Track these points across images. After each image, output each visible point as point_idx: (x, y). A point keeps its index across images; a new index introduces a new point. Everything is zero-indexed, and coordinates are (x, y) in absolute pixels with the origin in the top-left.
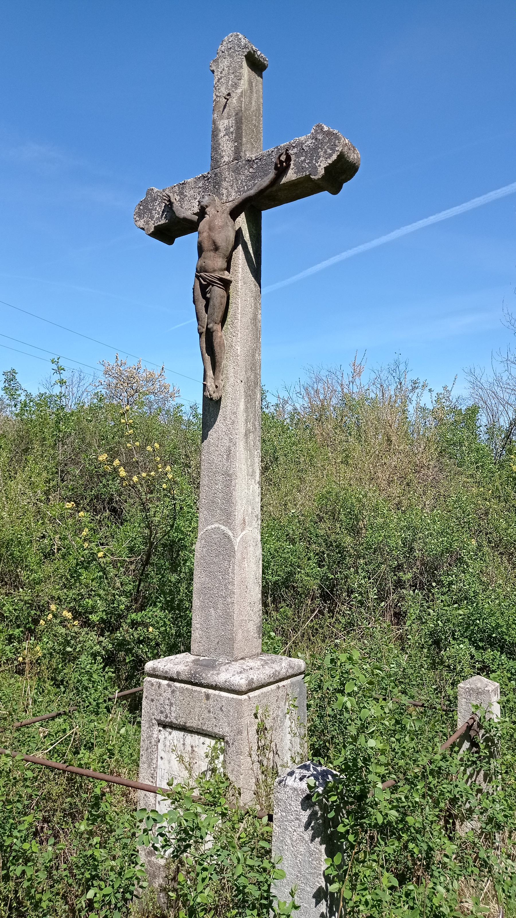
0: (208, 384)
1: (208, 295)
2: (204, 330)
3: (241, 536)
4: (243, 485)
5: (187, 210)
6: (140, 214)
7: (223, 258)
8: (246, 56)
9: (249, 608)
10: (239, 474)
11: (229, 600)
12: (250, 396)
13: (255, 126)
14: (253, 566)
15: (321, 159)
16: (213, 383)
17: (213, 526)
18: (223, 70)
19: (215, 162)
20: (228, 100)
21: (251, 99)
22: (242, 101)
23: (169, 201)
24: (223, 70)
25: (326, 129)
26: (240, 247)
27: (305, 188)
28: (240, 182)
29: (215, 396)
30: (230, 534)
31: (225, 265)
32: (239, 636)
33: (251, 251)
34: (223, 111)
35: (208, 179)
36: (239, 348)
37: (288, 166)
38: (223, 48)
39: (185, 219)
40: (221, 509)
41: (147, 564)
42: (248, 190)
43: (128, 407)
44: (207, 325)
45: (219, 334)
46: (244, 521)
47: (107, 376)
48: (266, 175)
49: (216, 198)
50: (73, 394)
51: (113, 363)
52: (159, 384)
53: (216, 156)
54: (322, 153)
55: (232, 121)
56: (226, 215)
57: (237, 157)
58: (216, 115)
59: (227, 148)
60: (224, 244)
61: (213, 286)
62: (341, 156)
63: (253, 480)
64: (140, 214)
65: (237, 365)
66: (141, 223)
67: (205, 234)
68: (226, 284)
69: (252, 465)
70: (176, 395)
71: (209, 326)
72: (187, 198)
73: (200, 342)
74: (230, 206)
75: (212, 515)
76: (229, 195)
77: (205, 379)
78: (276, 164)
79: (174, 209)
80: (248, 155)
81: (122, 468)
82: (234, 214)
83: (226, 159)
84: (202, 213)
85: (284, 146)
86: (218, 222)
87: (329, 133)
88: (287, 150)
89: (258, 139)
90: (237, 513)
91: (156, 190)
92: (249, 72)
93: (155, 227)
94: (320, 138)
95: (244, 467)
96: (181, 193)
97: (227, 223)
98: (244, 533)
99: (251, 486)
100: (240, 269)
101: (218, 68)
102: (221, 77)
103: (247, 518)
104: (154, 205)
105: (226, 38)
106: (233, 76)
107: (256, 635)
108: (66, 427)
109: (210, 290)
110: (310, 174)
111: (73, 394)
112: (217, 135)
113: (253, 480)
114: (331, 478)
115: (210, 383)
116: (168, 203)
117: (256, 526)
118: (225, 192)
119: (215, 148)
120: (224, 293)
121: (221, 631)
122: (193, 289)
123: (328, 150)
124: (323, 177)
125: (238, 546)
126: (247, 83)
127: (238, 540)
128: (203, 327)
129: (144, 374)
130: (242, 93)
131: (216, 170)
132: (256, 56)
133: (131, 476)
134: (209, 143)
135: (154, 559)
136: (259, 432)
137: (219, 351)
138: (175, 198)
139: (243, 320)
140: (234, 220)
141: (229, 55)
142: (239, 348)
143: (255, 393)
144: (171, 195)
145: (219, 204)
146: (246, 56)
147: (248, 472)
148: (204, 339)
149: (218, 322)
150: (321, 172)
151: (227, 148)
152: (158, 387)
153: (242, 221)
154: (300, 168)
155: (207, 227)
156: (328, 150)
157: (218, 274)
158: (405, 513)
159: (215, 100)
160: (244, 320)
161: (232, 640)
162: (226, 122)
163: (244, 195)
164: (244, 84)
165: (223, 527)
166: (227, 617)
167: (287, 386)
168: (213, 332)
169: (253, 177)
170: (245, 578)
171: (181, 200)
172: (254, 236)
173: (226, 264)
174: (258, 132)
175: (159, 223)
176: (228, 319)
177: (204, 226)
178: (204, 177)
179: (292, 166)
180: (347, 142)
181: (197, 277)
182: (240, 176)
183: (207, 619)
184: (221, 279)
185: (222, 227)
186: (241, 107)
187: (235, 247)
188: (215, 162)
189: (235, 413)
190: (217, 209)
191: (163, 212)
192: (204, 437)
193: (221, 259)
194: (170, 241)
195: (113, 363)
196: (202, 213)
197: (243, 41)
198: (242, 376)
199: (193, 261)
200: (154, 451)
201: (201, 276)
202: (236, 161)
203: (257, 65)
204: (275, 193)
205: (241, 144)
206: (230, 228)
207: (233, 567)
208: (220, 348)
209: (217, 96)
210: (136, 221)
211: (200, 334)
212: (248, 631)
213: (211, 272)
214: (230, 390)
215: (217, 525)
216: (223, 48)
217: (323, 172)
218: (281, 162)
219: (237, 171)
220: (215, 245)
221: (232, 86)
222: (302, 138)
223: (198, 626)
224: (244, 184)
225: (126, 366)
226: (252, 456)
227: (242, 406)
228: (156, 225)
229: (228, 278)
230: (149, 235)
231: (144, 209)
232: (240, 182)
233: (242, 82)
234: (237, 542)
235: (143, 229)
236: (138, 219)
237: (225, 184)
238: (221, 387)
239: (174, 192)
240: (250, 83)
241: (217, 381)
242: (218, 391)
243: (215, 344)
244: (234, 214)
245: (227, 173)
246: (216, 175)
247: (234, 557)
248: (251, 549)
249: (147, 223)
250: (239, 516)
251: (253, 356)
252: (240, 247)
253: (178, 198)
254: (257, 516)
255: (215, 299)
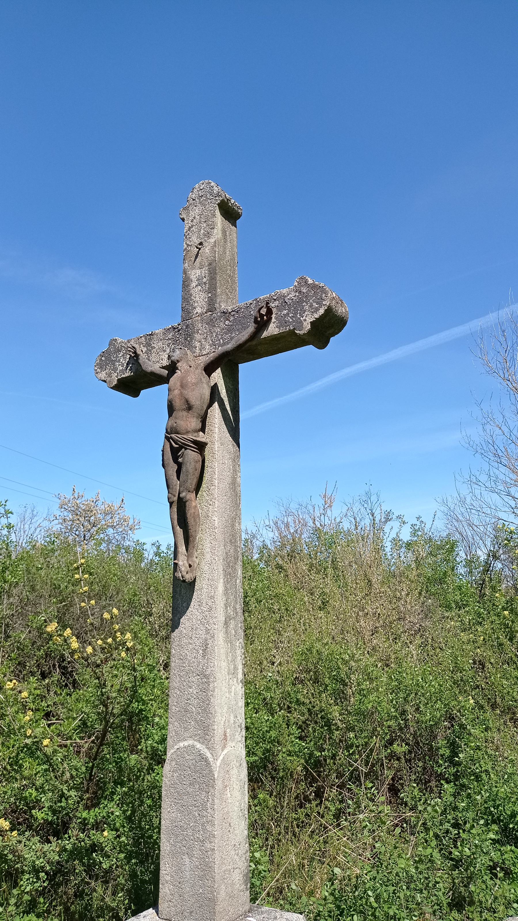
0: (180, 563)
1: (180, 460)
2: (176, 499)
3: (221, 758)
4: (223, 688)
5: (155, 362)
6: (101, 366)
7: (197, 418)
8: (218, 204)
9: (233, 852)
10: (218, 675)
11: (208, 845)
12: (230, 574)
13: (230, 276)
14: (237, 794)
15: (306, 313)
16: (185, 562)
17: (186, 743)
18: (194, 218)
19: (187, 312)
20: (200, 249)
21: (225, 248)
22: (215, 251)
23: (135, 352)
24: (194, 218)
25: (310, 281)
26: (216, 405)
27: (288, 341)
28: (214, 334)
29: (188, 577)
30: (208, 755)
31: (200, 425)
32: (222, 894)
33: (228, 408)
34: (195, 260)
35: (179, 331)
36: (216, 519)
37: (269, 319)
38: (194, 196)
39: (153, 374)
40: (196, 721)
41: (101, 744)
42: (224, 344)
43: (83, 561)
44: (179, 494)
45: (194, 504)
46: (225, 735)
47: (63, 510)
48: (245, 328)
49: (188, 352)
50: (24, 532)
51: (69, 496)
52: (118, 516)
53: (187, 307)
54: (307, 307)
55: (205, 271)
56: (200, 371)
57: (211, 307)
58: (186, 265)
59: (199, 300)
60: (198, 403)
61: (186, 449)
62: (329, 311)
63: (235, 679)
64: (101, 366)
65: (215, 539)
66: (103, 375)
67: (176, 392)
68: (201, 447)
69: (234, 660)
70: (136, 527)
71: (181, 495)
72: (155, 350)
73: (171, 512)
74: (204, 360)
75: (185, 728)
76: (202, 348)
77: (175, 557)
78: (256, 318)
79: (140, 361)
80: (223, 307)
81: (74, 638)
82: (209, 369)
83: (199, 310)
84: (172, 368)
85: (264, 299)
86: (191, 379)
87: (314, 287)
88: (268, 303)
89: (233, 290)
90: (216, 727)
91: (120, 340)
92: (222, 221)
93: (118, 380)
94: (304, 291)
95: (224, 664)
96: (148, 345)
97: (201, 379)
98: (225, 751)
99: (233, 688)
100: (217, 429)
101: (188, 215)
102: (192, 226)
103: (228, 730)
104: (117, 357)
105: (197, 186)
106: (205, 225)
107: (243, 887)
108: (12, 577)
109: (182, 454)
110: (294, 329)
111: (24, 532)
112: (188, 285)
113: (235, 679)
114: (315, 630)
115: (182, 562)
116: (133, 355)
117: (240, 739)
118: (197, 344)
119: (187, 298)
120: (199, 457)
121: (197, 888)
122: (163, 451)
123: (314, 304)
124: (309, 332)
125: (219, 772)
126: (220, 235)
127: (218, 763)
128: (175, 496)
129: (103, 507)
130: (215, 242)
131: (187, 322)
132: (230, 204)
133: (84, 647)
134: (180, 294)
135: (110, 737)
136: (241, 618)
137: (193, 523)
138: (141, 350)
139: (221, 486)
140: (209, 375)
141: (200, 203)
142: (216, 519)
143: (235, 569)
144: (136, 346)
145: (192, 358)
146: (218, 204)
147: (229, 670)
148: (175, 509)
149: (193, 489)
150: (307, 327)
151: (199, 300)
152: (117, 520)
153: (218, 376)
154: (282, 322)
155: (179, 384)
156: (314, 304)
157: (191, 437)
158: (398, 665)
159: (186, 249)
160: (221, 486)
161: (213, 901)
162: (198, 272)
163: (220, 350)
164: (217, 233)
165: (198, 746)
166: (206, 869)
167: (261, 525)
168: (187, 501)
169: (229, 330)
170: (228, 812)
171: (149, 352)
172: (231, 392)
173: (201, 424)
174: (233, 282)
175: (123, 376)
176: (204, 485)
177: (175, 384)
178: (174, 328)
179: (273, 320)
180: (334, 296)
181: (166, 437)
182: (215, 328)
183: (180, 870)
184: (195, 442)
185: (195, 382)
186: (215, 257)
187: (210, 405)
188: (187, 312)
189: (212, 597)
190: (190, 363)
191: (127, 364)
192: (175, 624)
193: (195, 419)
194: (135, 393)
195: (69, 496)
196: (172, 368)
197: (216, 189)
198: (220, 551)
199: (162, 420)
200: (112, 618)
201: (171, 438)
202: (210, 313)
203: (230, 214)
204: (254, 348)
205: (215, 295)
206: (205, 386)
207: (213, 800)
208: (195, 520)
209: (188, 245)
210: (97, 373)
211: (171, 504)
212: (233, 884)
213: (184, 434)
214: (206, 568)
215: (190, 742)
216: (194, 196)
217: (309, 327)
218: (262, 316)
219: (211, 323)
220: (188, 404)
221: (205, 235)
222: (285, 291)
223: (168, 878)
224: (220, 337)
225: (83, 499)
226: (233, 648)
227: (221, 588)
228: (119, 377)
229: (203, 440)
230: (111, 388)
231: (106, 360)
232: (214, 334)
233: (215, 231)
234: (217, 765)
235: (105, 381)
236: (99, 370)
237: (197, 336)
238: (196, 565)
239: (140, 344)
240: (224, 232)
241: (190, 559)
242: (192, 571)
243: (188, 515)
244: (209, 369)
245: (200, 325)
246: (187, 326)
247: (213, 787)
248: (235, 771)
249: (110, 375)
250: (218, 730)
251: (233, 526)
252: (216, 405)
253: (144, 350)
254: (240, 726)
255: (188, 464)
